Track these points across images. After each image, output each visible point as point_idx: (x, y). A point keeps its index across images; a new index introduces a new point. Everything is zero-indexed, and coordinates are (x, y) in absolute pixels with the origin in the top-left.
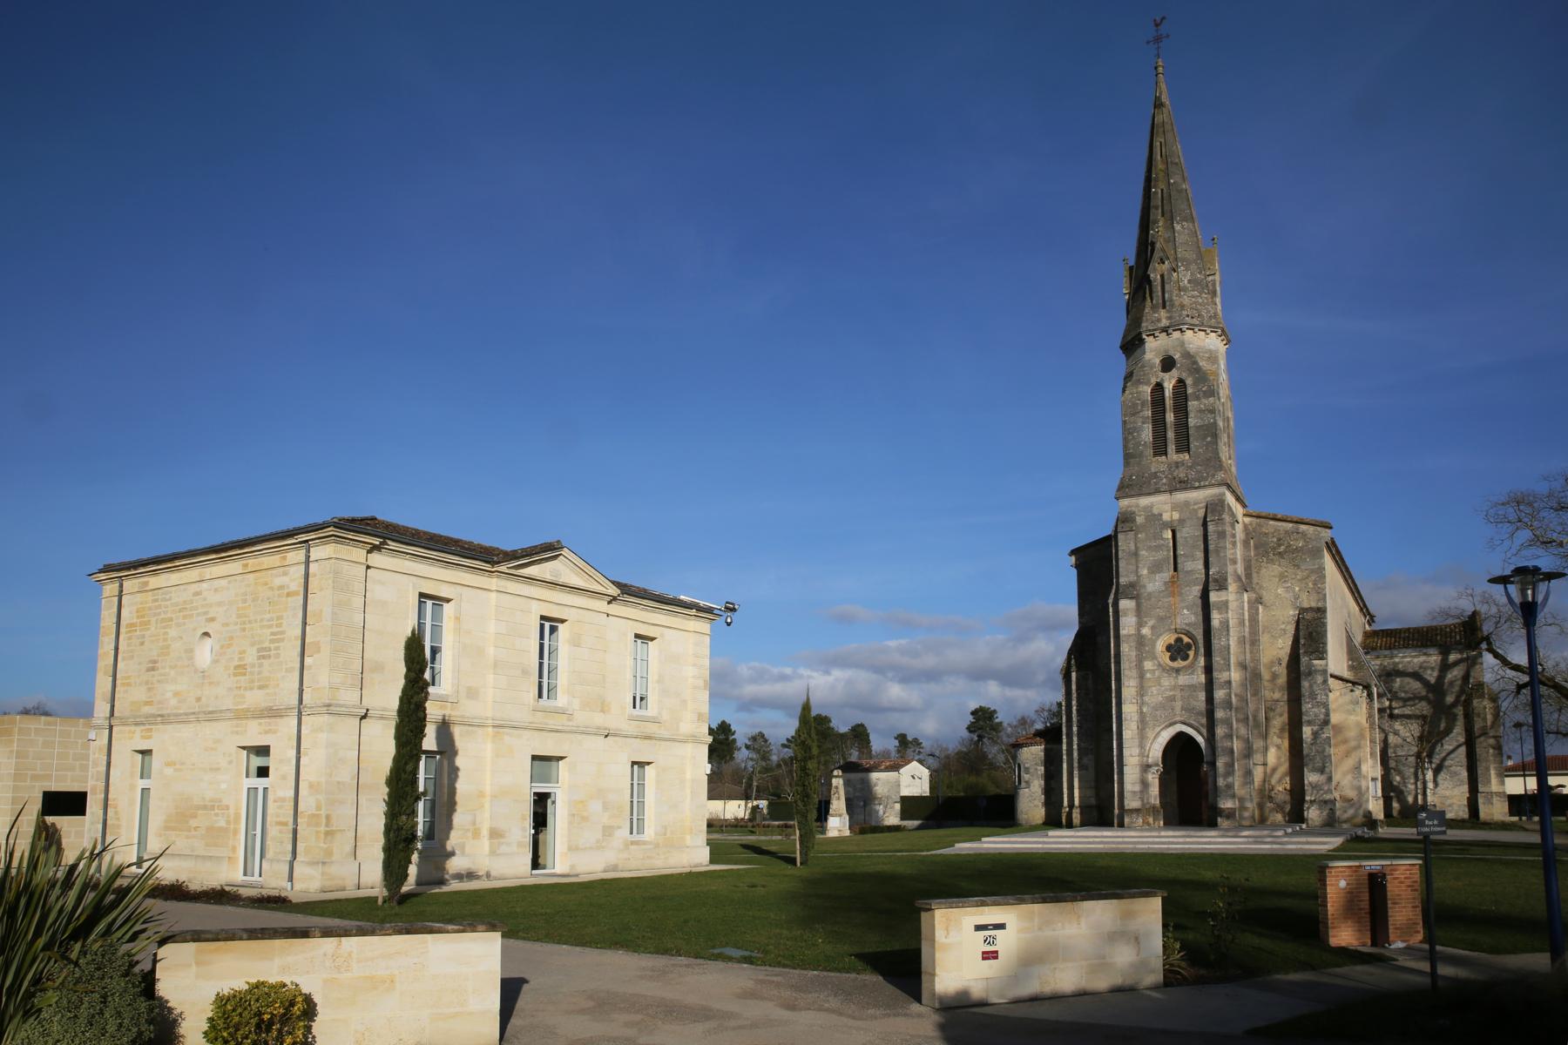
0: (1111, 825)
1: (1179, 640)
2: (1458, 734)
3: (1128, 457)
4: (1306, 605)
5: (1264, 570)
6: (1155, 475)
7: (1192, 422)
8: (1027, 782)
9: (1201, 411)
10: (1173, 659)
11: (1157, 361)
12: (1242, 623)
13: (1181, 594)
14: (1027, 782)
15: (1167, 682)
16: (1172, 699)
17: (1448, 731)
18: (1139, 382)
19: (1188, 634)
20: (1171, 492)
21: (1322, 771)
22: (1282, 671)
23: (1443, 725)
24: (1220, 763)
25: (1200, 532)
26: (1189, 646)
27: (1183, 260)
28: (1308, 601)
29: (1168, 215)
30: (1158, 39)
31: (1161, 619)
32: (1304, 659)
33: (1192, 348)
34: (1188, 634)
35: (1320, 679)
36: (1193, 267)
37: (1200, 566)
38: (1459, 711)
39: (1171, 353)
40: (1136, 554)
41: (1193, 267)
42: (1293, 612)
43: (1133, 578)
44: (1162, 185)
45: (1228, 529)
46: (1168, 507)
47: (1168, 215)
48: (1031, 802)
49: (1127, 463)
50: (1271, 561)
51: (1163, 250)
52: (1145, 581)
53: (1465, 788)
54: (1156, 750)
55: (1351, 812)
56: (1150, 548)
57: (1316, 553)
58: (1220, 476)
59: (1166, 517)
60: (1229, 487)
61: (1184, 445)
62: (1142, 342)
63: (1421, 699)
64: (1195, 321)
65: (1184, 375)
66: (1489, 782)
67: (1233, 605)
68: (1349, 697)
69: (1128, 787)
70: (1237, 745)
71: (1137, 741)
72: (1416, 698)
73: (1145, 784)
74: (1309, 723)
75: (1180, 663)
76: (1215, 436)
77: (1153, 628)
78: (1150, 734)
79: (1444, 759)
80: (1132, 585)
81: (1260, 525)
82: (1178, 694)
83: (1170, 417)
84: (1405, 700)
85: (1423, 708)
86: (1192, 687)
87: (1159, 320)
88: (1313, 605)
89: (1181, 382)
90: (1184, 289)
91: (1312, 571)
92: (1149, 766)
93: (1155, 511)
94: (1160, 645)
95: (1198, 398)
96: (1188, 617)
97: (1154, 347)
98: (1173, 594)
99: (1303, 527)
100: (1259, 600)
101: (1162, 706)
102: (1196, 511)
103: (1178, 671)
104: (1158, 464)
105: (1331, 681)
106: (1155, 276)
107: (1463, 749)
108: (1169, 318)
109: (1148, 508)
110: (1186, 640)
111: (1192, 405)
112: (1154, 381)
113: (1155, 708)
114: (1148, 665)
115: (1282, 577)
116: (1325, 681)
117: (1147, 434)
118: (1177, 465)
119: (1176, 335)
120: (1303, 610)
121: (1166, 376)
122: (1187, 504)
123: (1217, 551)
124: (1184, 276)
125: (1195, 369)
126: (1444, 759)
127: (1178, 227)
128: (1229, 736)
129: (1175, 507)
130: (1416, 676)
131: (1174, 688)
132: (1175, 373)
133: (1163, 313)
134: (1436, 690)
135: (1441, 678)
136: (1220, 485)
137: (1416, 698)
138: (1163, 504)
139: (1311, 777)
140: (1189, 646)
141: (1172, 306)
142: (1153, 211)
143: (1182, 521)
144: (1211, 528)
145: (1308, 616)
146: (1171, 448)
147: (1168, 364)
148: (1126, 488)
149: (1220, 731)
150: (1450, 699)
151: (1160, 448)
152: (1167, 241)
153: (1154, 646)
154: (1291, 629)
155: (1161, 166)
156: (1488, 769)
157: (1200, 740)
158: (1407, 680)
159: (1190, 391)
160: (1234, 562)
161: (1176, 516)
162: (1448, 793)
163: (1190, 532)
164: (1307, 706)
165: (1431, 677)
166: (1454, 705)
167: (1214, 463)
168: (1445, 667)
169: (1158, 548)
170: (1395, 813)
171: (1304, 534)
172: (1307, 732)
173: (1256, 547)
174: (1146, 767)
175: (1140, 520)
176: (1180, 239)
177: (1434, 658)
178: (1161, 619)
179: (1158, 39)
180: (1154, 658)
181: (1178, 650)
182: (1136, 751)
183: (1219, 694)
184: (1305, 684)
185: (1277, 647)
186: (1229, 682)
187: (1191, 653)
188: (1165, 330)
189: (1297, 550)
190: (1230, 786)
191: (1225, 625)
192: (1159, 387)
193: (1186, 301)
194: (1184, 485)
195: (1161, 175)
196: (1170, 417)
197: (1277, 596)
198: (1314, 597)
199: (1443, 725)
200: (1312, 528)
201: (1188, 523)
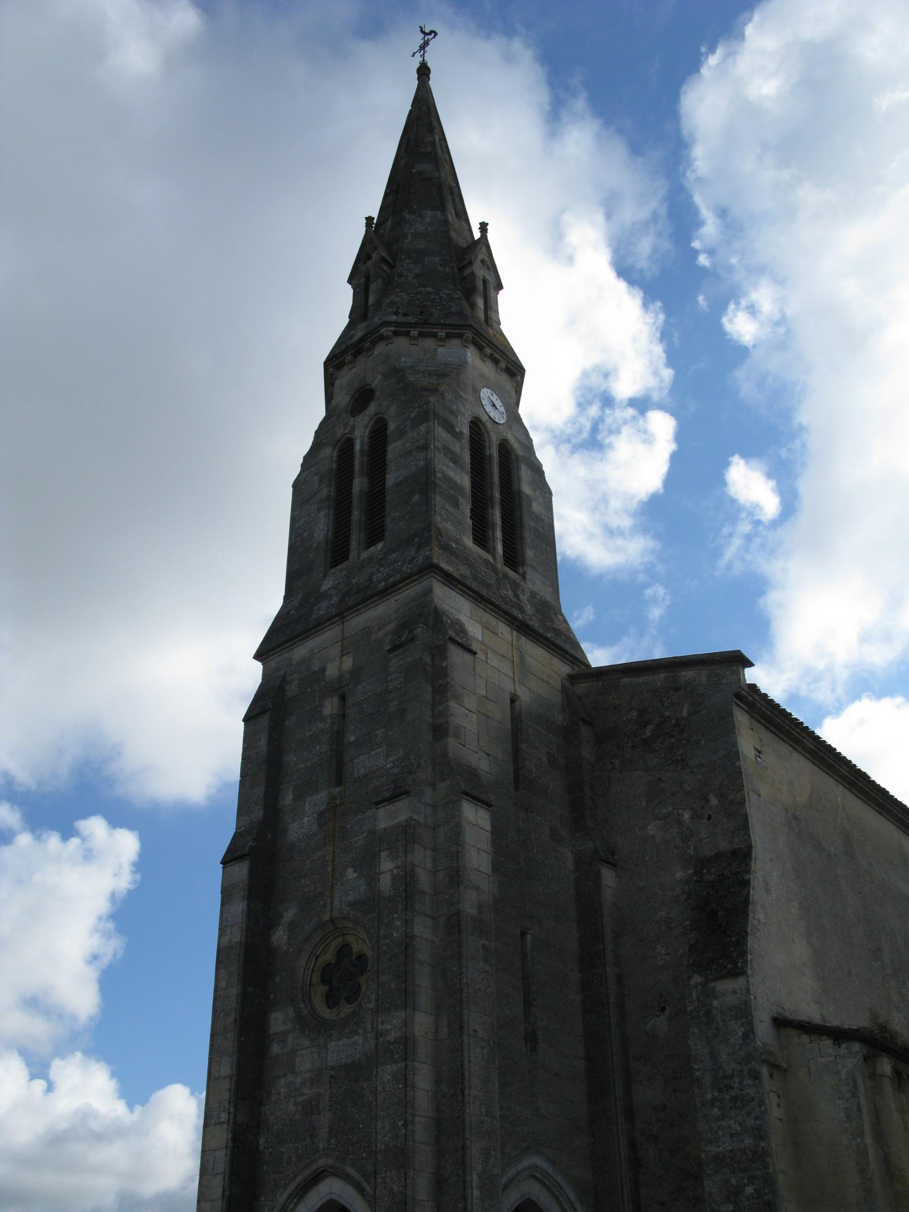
61: (375, 534)
88: (724, 845)
111: (394, 449)
143: (356, 673)
146: (356, 538)
159: (392, 426)
196: (359, 484)
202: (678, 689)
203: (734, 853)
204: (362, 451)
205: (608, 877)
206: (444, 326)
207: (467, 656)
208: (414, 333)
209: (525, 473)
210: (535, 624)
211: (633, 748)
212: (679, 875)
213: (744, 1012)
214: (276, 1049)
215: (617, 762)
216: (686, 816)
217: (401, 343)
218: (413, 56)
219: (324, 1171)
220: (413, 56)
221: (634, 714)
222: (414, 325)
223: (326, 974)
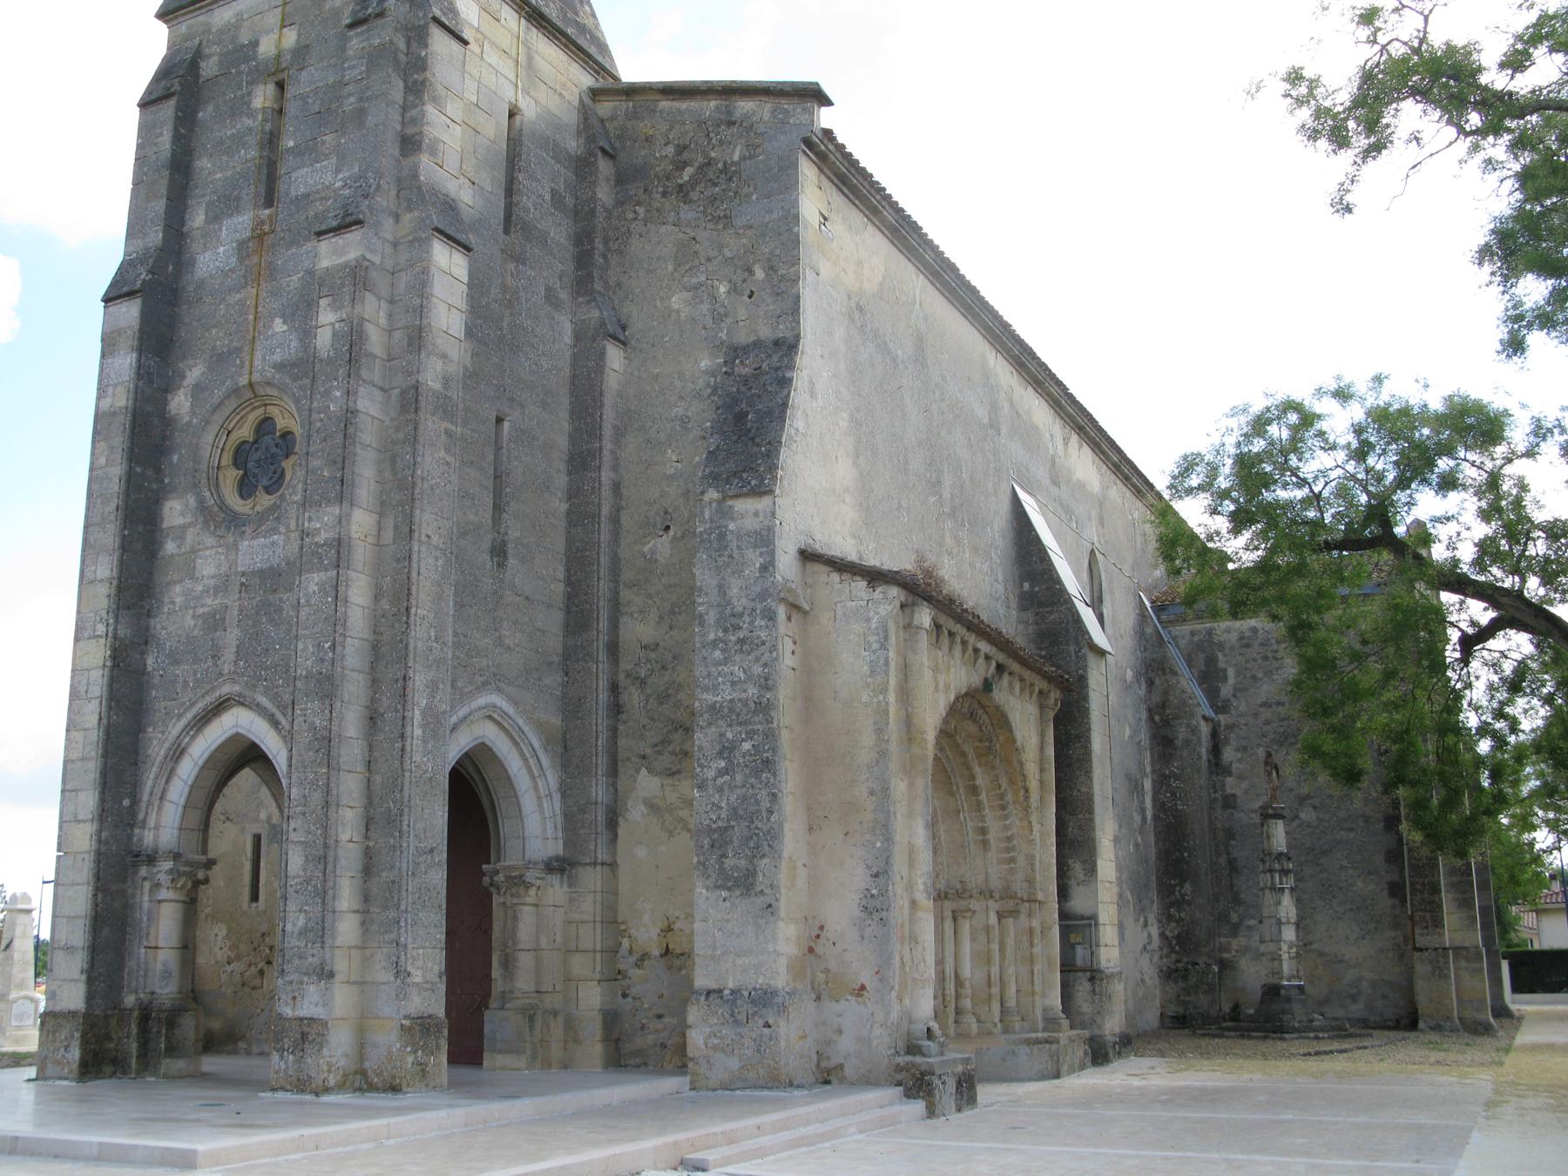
4: (743, 337)
13: (272, 271)
59: (267, 48)
88: (765, 332)
114: (175, 512)
120: (736, 352)
131: (222, 587)
143: (301, 53)
202: (731, 124)
205: (615, 357)
207: (455, 46)
213: (765, 539)
215: (641, 210)
223: (241, 455)
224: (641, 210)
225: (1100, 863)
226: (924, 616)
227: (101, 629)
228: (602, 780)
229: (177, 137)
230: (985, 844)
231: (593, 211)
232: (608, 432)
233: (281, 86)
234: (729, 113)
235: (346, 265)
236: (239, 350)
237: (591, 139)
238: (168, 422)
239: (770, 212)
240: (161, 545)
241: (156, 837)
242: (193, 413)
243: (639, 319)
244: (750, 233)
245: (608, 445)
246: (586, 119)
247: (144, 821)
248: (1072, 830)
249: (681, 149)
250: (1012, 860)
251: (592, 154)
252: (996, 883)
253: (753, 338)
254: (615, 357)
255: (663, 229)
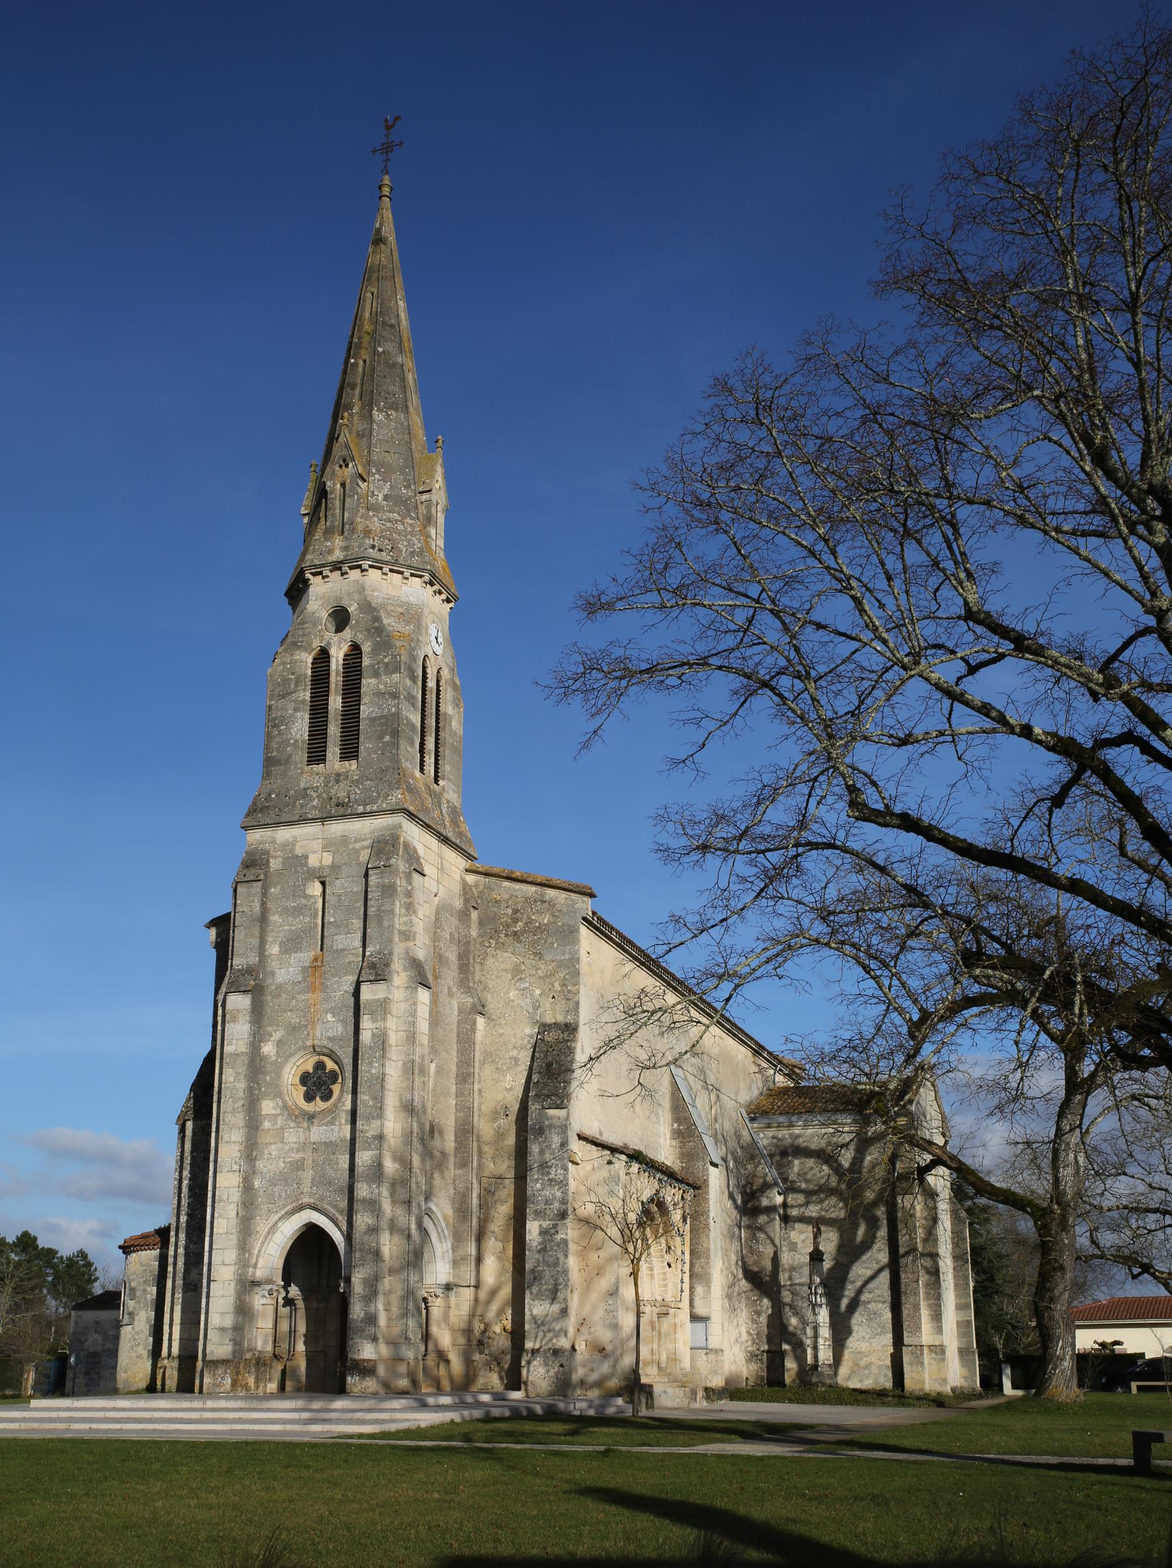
0: (192, 1391)
1: (320, 1066)
2: (879, 1254)
3: (270, 762)
4: (549, 1020)
5: (490, 961)
6: (304, 793)
7: (365, 711)
8: (131, 1314)
9: (379, 694)
10: (309, 1097)
11: (324, 614)
12: (411, 1038)
13: (324, 988)
14: (131, 1314)
15: (293, 1136)
16: (299, 1166)
17: (867, 1245)
18: (295, 646)
19: (331, 1055)
20: (323, 820)
21: (554, 1295)
22: (508, 1124)
23: (861, 1232)
24: (358, 1278)
25: (359, 888)
26: (333, 1077)
27: (380, 465)
28: (553, 1014)
29: (366, 398)
30: (387, 148)
31: (293, 1029)
32: (534, 1107)
33: (376, 597)
34: (331, 1055)
35: (556, 1140)
36: (397, 477)
37: (358, 943)
38: (881, 1212)
39: (345, 603)
40: (263, 919)
41: (397, 477)
42: (529, 1030)
43: (253, 959)
44: (365, 354)
45: (401, 882)
46: (317, 845)
47: (366, 398)
48: (133, 1359)
49: (267, 775)
50: (501, 946)
51: (347, 446)
52: (273, 965)
53: (888, 1338)
54: (271, 1253)
55: (605, 1368)
56: (286, 911)
57: (569, 936)
58: (397, 796)
59: (313, 861)
60: (411, 816)
61: (350, 751)
62: (306, 583)
63: (832, 1192)
64: (384, 556)
65: (360, 638)
66: (918, 1328)
67: (398, 1007)
68: (604, 1173)
69: (215, 1320)
70: (389, 1246)
71: (234, 1239)
72: (820, 1191)
73: (243, 1311)
74: (538, 1214)
75: (319, 1105)
76: (396, 734)
77: (280, 1043)
78: (261, 1226)
79: (859, 1292)
80: (250, 971)
81: (489, 887)
82: (308, 1156)
83: (336, 702)
84: (808, 1193)
85: (836, 1209)
86: (330, 1146)
87: (330, 552)
88: (560, 1019)
89: (356, 648)
90: (376, 508)
91: (561, 964)
92: (255, 1284)
93: (299, 851)
94: (290, 1075)
95: (376, 674)
96: (331, 1027)
97: (322, 593)
98: (312, 988)
99: (551, 893)
100: (480, 1009)
101: (282, 1178)
102: (357, 852)
103: (311, 1117)
104: (312, 777)
105: (576, 1146)
106: (334, 486)
107: (885, 1276)
108: (346, 549)
109: (289, 845)
110: (330, 1065)
111: (368, 684)
112: (316, 644)
113: (272, 1182)
114: (268, 1106)
115: (517, 972)
116: (564, 1144)
117: (300, 727)
118: (338, 777)
119: (354, 575)
120: (544, 1027)
121: (336, 638)
122: (345, 840)
123: (379, 918)
124: (378, 489)
125: (377, 630)
126: (859, 1292)
127: (378, 416)
128: (374, 1230)
129: (329, 845)
130: (825, 1156)
131: (302, 1147)
132: (347, 633)
133: (338, 541)
134: (849, 1183)
135: (857, 1161)
136: (393, 811)
137: (820, 1191)
138: (309, 841)
139: (536, 1308)
140: (333, 1077)
141: (353, 531)
142: (348, 390)
143: (335, 868)
144: (373, 879)
145: (550, 1037)
146: (333, 750)
147: (341, 618)
148: (261, 813)
149: (363, 1220)
150: (870, 1195)
151: (317, 754)
152: (360, 435)
153: (278, 1075)
154: (525, 1057)
155: (367, 327)
156: (917, 1307)
157: (337, 1237)
158: (810, 1162)
159: (366, 662)
160: (407, 936)
161: (328, 859)
162: (864, 1347)
163: (347, 885)
164: (535, 1185)
165: (846, 1158)
166: (875, 1204)
167: (393, 775)
168: (863, 1144)
169: (298, 910)
170: (789, 1378)
171: (551, 904)
172: (533, 1228)
173: (481, 923)
174: (247, 1285)
175: (275, 864)
176: (379, 434)
177: (846, 1128)
178: (293, 1029)
179: (387, 148)
180: (279, 1095)
181: (317, 1084)
182: (231, 1255)
183: (364, 1157)
184: (534, 1148)
185: (502, 1085)
186: (381, 1137)
187: (336, 1088)
188: (337, 567)
189: (541, 929)
190: (371, 1319)
191: (382, 1041)
192: (323, 657)
193: (375, 524)
194: (341, 810)
195: (366, 339)
196: (336, 702)
197: (508, 1002)
198: (561, 1005)
199: (861, 1232)
200: (563, 895)
201: (345, 871)
202: (543, 902)
203: (567, 1025)
204: (337, 671)
205: (481, 1022)
206: (410, 567)
207: (421, 878)
208: (386, 569)
209: (741, 1426)
210: (450, 835)
211: (506, 935)
212: (528, 1031)
213: (564, 1128)
214: (267, 1124)
215: (493, 942)
216: (538, 992)
217: (374, 574)
218: (374, 152)
219: (581, 1220)
220: (374, 152)
221: (510, 911)
222: (386, 563)
223: (305, 1079)
224: (493, 942)
225: (713, 1288)
226: (635, 1167)
227: (236, 1167)
228: (474, 1244)
229: (518, 1136)
230: (652, 1276)
231: (469, 942)
232: (477, 1064)
233: (323, 883)
234: (542, 895)
235: (378, 1000)
236: (306, 1026)
237: (466, 901)
238: (263, 1058)
239: (564, 954)
240: (261, 1123)
241: (254, 1273)
242: (278, 1054)
243: (493, 1003)
244: (554, 964)
245: (477, 1071)
246: (464, 889)
247: (256, 1264)
248: (698, 1269)
249: (516, 911)
250: (666, 1285)
251: (468, 910)
252: (659, 1298)
253: (553, 1021)
254: (481, 1022)
255: (506, 954)
